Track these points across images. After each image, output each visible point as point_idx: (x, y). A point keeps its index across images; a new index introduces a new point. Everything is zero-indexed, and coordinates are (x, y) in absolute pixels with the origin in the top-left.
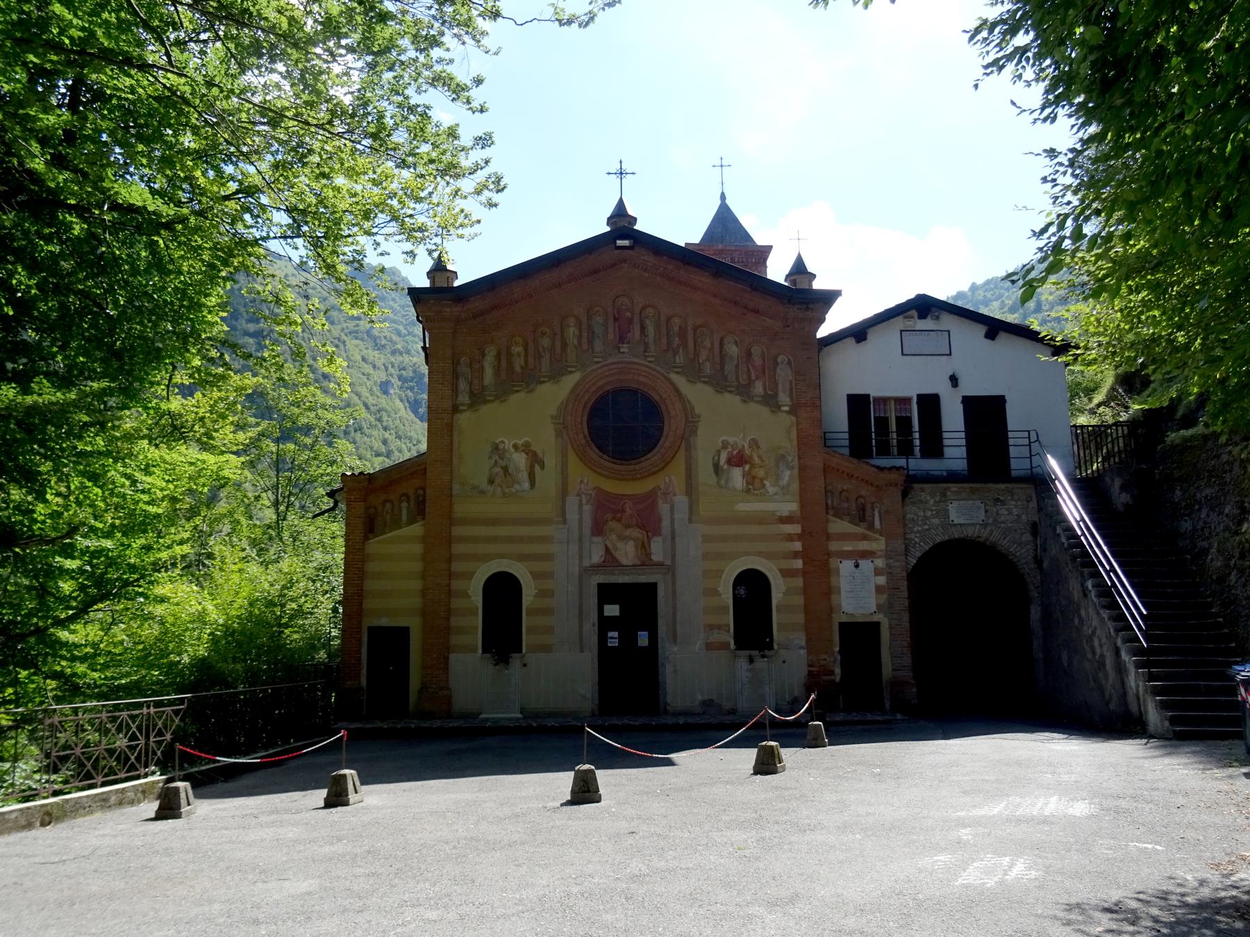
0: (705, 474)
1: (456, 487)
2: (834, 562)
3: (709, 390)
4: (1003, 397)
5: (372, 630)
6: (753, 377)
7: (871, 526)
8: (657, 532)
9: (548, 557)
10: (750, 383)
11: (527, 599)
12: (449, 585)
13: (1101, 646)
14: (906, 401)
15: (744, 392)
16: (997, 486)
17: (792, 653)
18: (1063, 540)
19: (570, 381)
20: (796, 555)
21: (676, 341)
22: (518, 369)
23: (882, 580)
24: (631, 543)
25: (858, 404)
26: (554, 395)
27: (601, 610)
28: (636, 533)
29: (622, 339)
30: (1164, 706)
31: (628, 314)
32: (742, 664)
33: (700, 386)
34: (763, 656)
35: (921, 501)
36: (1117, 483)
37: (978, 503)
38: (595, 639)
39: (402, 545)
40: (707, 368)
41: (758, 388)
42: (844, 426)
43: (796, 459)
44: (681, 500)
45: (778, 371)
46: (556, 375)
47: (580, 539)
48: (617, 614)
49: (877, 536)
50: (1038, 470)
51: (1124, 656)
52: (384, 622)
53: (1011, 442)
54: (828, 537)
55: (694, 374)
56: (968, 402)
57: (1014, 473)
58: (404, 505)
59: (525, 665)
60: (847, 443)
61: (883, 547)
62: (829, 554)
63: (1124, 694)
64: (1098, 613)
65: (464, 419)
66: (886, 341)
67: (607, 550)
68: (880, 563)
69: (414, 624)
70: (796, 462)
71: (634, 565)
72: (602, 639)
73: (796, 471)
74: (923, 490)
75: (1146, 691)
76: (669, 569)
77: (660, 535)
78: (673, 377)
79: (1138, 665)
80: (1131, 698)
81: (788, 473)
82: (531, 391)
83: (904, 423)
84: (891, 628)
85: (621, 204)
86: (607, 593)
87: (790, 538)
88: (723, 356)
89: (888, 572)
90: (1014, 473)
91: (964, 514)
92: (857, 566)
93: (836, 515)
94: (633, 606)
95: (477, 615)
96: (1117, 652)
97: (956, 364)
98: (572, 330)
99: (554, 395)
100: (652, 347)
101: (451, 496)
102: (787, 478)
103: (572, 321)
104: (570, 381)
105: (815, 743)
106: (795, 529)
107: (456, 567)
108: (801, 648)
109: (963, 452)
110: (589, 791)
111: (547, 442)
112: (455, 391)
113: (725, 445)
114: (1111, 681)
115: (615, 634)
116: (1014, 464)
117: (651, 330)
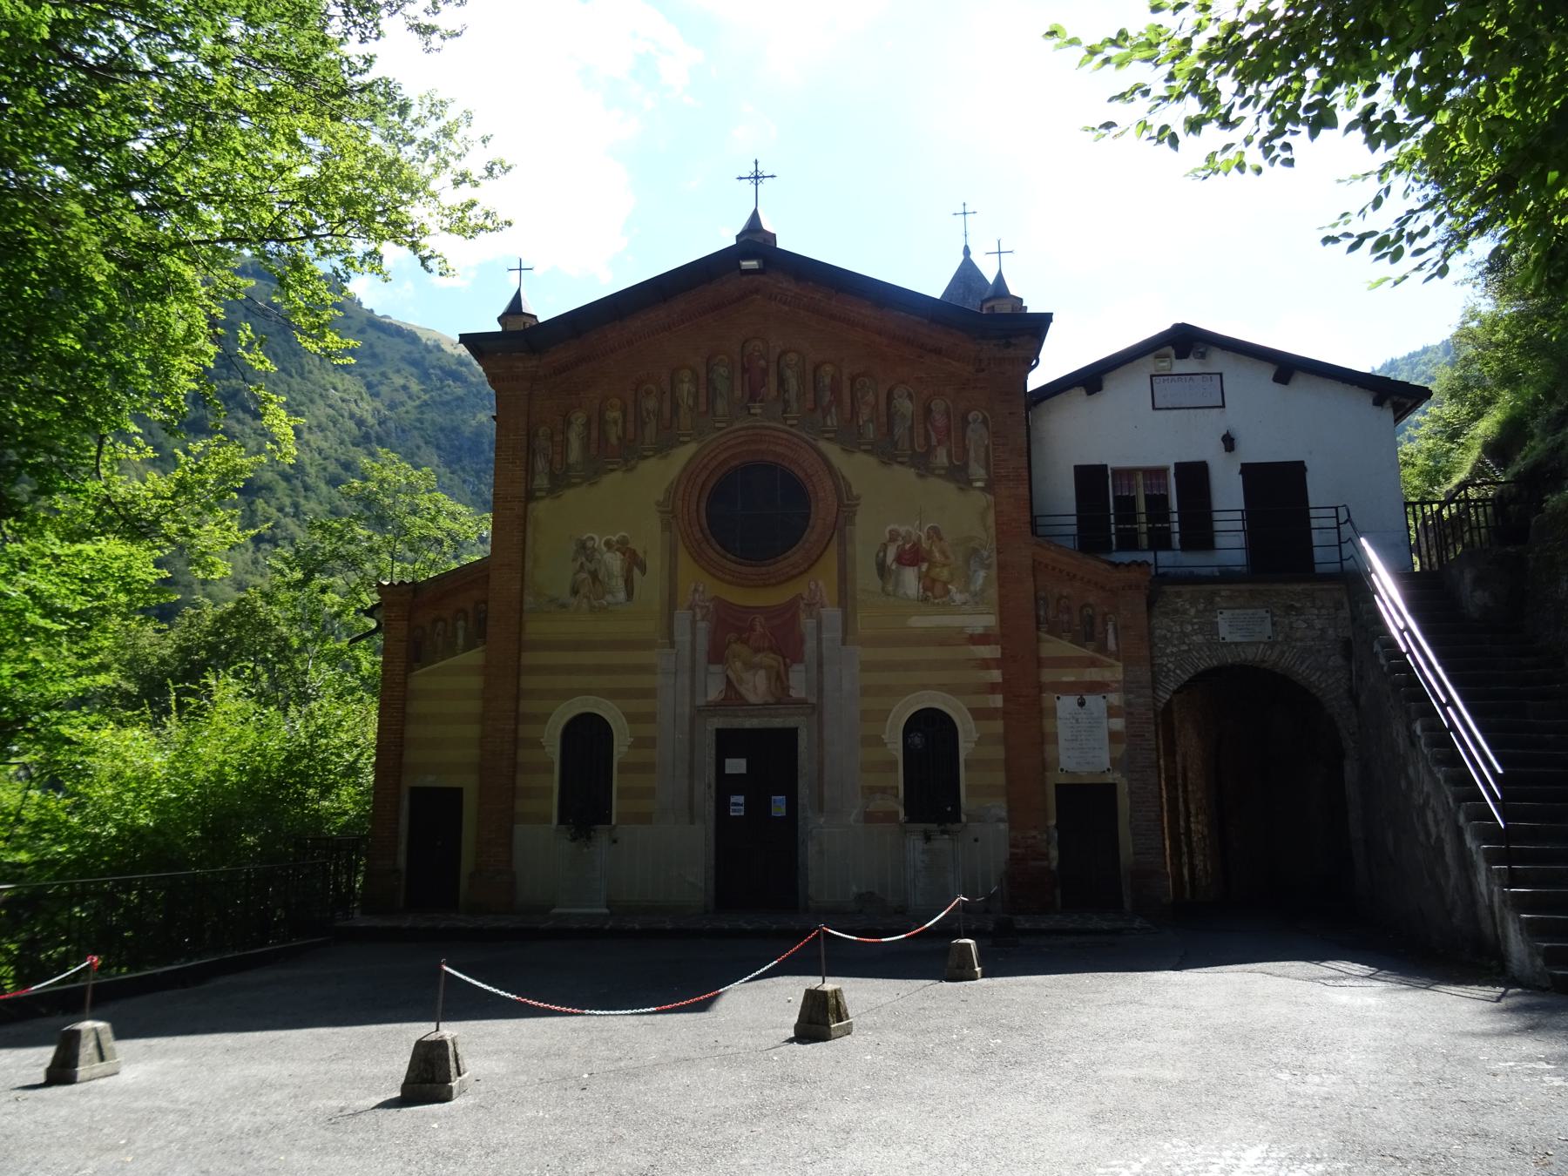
0: (865, 578)
1: (529, 600)
2: (1048, 698)
3: (872, 461)
4: (1302, 463)
5: (416, 792)
6: (934, 442)
7: (1102, 648)
8: (798, 657)
9: (648, 693)
10: (930, 451)
11: (621, 748)
12: (516, 731)
13: (1437, 824)
14: (1160, 473)
15: (922, 463)
16: (1290, 587)
17: (988, 831)
18: (1383, 661)
19: (683, 454)
20: (993, 688)
21: (827, 397)
22: (614, 440)
23: (1118, 724)
24: (762, 673)
25: (1090, 478)
26: (660, 474)
27: (720, 766)
28: (769, 659)
29: (753, 397)
30: (1533, 931)
31: (762, 363)
32: (916, 844)
33: (860, 457)
34: (943, 832)
35: (1176, 611)
36: (1468, 576)
37: (1262, 612)
38: (710, 807)
39: (456, 679)
40: (871, 431)
41: (941, 457)
42: (1071, 507)
43: (994, 555)
44: (832, 614)
45: (969, 433)
46: (663, 448)
47: (693, 670)
48: (743, 770)
49: (1112, 661)
50: (1347, 564)
51: (1470, 843)
52: (430, 781)
53: (1314, 523)
54: (1040, 663)
55: (851, 439)
56: (1248, 471)
57: (1319, 569)
58: (461, 623)
59: (615, 841)
60: (1074, 530)
61: (1120, 677)
62: (1041, 688)
63: (1473, 902)
64: (1431, 773)
65: (541, 509)
66: (1129, 391)
67: (729, 682)
68: (1115, 699)
69: (468, 782)
70: (994, 559)
71: (766, 704)
72: (722, 805)
73: (994, 572)
74: (1179, 595)
75: (1504, 902)
76: (815, 710)
77: (801, 661)
78: (823, 445)
79: (1491, 858)
80: (1483, 912)
81: (982, 573)
82: (630, 470)
83: (1157, 504)
84: (1131, 792)
85: (755, 216)
86: (728, 742)
87: (986, 664)
88: (890, 417)
89: (1126, 711)
90: (1319, 569)
91: (1239, 629)
92: (1082, 704)
93: (1049, 632)
94: (765, 759)
95: (551, 771)
96: (1459, 833)
97: (1231, 419)
98: (686, 386)
99: (660, 474)
100: (795, 406)
101: (521, 611)
102: (980, 582)
103: (686, 375)
104: (683, 454)
105: (959, 972)
106: (990, 652)
107: (527, 706)
108: (1001, 820)
109: (1239, 540)
110: (432, 1081)
111: (650, 537)
112: (530, 471)
113: (894, 536)
114: (1452, 882)
115: (741, 799)
116: (1318, 554)
117: (793, 384)
